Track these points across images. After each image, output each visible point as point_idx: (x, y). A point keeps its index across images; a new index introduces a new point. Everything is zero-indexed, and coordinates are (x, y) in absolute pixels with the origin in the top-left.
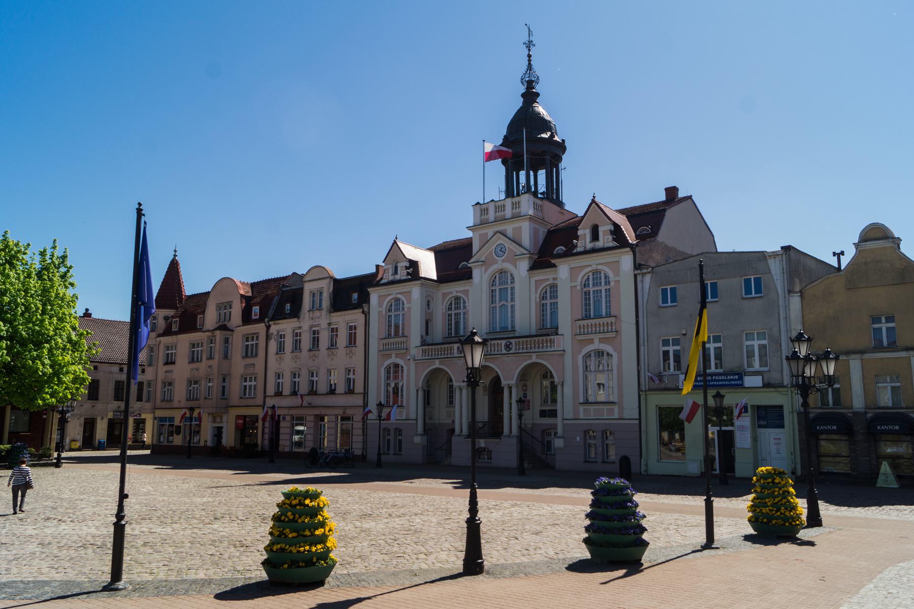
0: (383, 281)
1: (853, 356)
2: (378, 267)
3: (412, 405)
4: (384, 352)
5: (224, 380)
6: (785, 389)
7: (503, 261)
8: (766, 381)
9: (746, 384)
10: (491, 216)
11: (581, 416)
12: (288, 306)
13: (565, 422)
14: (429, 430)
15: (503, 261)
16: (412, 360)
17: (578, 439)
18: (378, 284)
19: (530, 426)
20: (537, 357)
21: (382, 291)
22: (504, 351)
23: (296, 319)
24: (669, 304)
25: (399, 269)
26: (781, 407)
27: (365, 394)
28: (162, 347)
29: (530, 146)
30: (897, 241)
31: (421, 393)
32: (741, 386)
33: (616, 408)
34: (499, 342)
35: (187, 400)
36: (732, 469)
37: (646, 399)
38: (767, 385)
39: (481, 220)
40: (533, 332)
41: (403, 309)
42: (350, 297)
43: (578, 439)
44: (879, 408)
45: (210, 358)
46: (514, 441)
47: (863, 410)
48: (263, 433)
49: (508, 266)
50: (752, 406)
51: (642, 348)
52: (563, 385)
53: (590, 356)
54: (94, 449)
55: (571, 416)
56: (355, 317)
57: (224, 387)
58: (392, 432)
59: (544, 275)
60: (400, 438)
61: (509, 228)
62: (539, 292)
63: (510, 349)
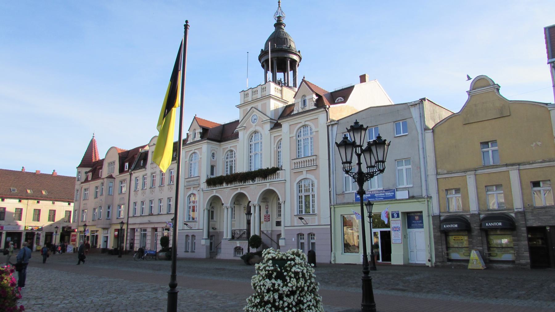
1: (469, 173)
4: (188, 188)
5: (109, 208)
6: (423, 200)
7: (256, 125)
8: (411, 195)
12: (142, 162)
13: (286, 228)
17: (293, 240)
19: (270, 232)
20: (216, 192)
23: (144, 169)
24: (402, 134)
26: (421, 212)
28: (83, 190)
30: (497, 88)
31: (206, 212)
32: (394, 196)
35: (93, 221)
36: (389, 259)
37: (334, 211)
38: (412, 197)
43: (293, 240)
44: (488, 210)
45: (102, 194)
47: (477, 212)
48: (127, 240)
49: (258, 128)
50: (403, 213)
55: (289, 224)
57: (109, 212)
58: (306, 236)
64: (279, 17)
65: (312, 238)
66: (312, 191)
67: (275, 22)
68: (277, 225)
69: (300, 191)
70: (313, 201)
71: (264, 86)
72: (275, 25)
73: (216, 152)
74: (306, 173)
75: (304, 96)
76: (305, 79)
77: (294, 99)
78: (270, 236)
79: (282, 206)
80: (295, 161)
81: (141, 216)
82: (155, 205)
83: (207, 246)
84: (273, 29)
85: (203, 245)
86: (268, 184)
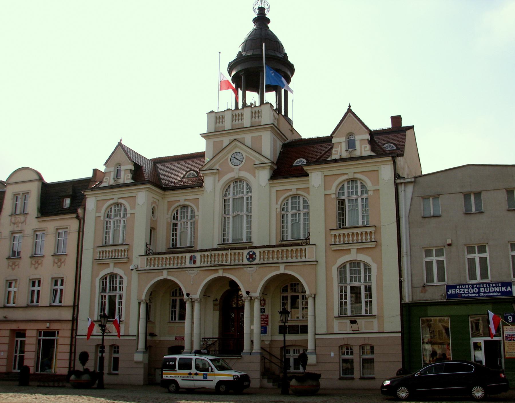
0: (103, 185)
2: (95, 171)
3: (132, 319)
4: (100, 262)
10: (228, 125)
11: (336, 331)
13: (317, 337)
14: (151, 348)
15: (240, 170)
16: (135, 270)
17: (332, 354)
18: (97, 188)
19: (267, 343)
21: (103, 195)
22: (246, 262)
25: (123, 173)
27: (75, 307)
29: (262, 63)
31: (143, 307)
33: (375, 321)
34: (241, 251)
39: (216, 128)
40: (274, 243)
41: (125, 215)
42: (61, 203)
43: (332, 354)
46: (258, 356)
49: (244, 174)
51: (405, 261)
52: (314, 298)
53: (345, 266)
55: (324, 331)
56: (71, 223)
58: (356, 350)
59: (291, 186)
60: (116, 355)
61: (248, 138)
62: (279, 203)
63: (254, 259)
64: (262, 10)
65: (115, 353)
66: (120, 290)
69: (104, 289)
70: (120, 303)
71: (257, 109)
72: (255, 20)
73: (157, 206)
74: (114, 267)
76: (123, 142)
77: (105, 167)
78: (268, 350)
79: (310, 302)
80: (101, 249)
81: (51, 306)
82: (46, 290)
83: (145, 364)
84: (252, 26)
85: (137, 363)
86: (165, 272)
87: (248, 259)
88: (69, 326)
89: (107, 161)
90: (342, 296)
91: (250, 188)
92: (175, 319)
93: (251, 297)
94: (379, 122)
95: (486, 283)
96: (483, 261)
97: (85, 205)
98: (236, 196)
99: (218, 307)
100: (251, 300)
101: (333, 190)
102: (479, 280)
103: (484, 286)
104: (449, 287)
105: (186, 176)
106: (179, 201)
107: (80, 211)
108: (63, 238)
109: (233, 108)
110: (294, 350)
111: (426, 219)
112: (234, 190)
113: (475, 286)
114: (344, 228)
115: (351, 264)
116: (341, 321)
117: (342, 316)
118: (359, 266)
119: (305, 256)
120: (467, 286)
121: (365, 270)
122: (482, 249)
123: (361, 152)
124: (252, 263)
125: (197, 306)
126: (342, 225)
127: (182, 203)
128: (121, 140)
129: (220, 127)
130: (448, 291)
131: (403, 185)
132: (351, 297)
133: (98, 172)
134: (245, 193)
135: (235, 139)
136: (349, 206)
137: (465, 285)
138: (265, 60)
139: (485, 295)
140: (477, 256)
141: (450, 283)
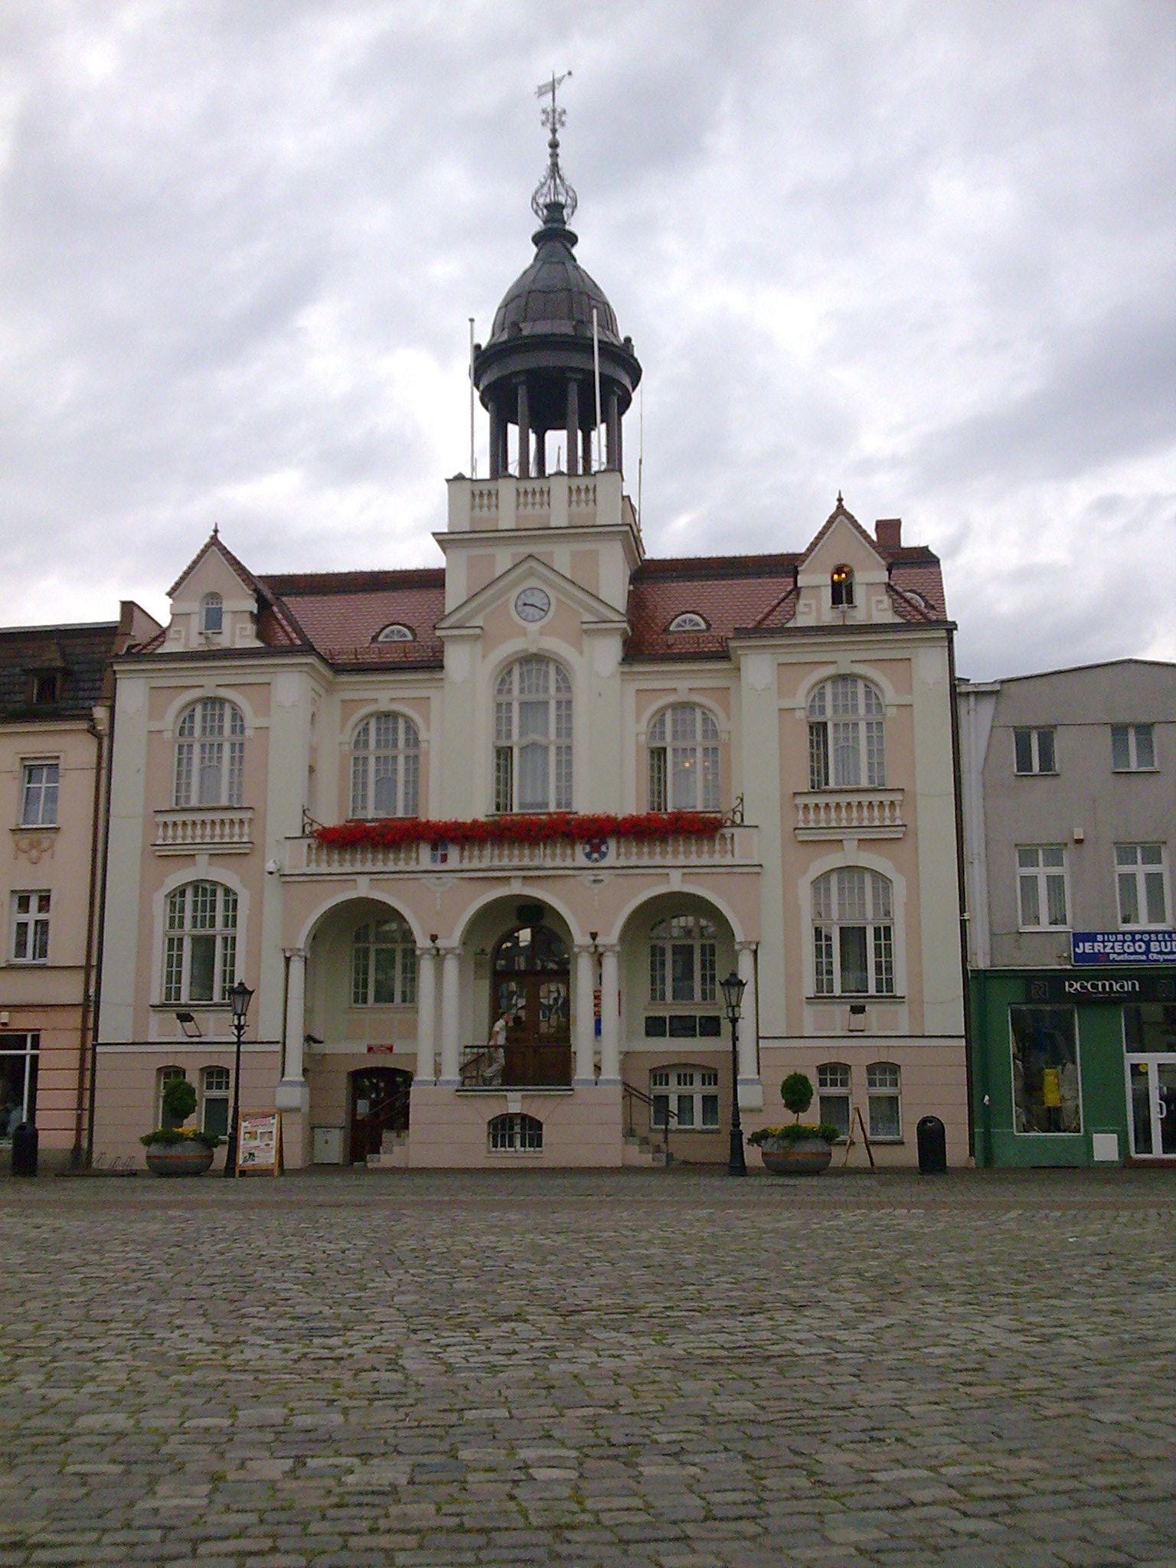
0: (168, 647)
9: (395, 1050)
16: (276, 875)
24: (1134, 767)
27: (92, 968)
29: (554, 364)
33: (903, 1010)
46: (619, 1089)
49: (552, 644)
52: (755, 952)
53: (183, 894)
54: (1059, 1131)
56: (72, 748)
61: (562, 556)
63: (603, 855)
67: (537, 225)
68: (648, 1034)
70: (230, 961)
72: (538, 239)
75: (214, 596)
84: (527, 254)
86: (363, 880)
87: (588, 856)
88: (75, 1018)
89: (178, 584)
90: (822, 948)
91: (565, 679)
92: (365, 1001)
93: (438, 950)
94: (909, 539)
95: (1163, 933)
96: (1155, 881)
97: (113, 698)
98: (527, 697)
99: (487, 972)
100: (438, 956)
101: (800, 699)
102: (1143, 924)
103: (1128, 937)
104: (1079, 938)
105: (380, 639)
106: (375, 700)
107: (100, 713)
108: (44, 785)
109: (484, 471)
110: (679, 1076)
111: (1123, 779)
112: (522, 681)
113: (1138, 937)
114: (825, 792)
115: (196, 888)
116: (820, 1007)
117: (822, 995)
118: (214, 893)
119: (732, 852)
120: (1120, 937)
121: (226, 902)
122: (1152, 854)
123: (870, 617)
124: (597, 865)
125: (610, 964)
126: (818, 786)
127: (384, 706)
128: (216, 531)
129: (477, 517)
130: (1076, 945)
131: (972, 698)
132: (674, 962)
133: (137, 613)
134: (552, 690)
135: (530, 556)
136: (836, 739)
137: (1116, 934)
138: (600, 355)
139: (1161, 957)
140: (1140, 870)
141: (1081, 929)
